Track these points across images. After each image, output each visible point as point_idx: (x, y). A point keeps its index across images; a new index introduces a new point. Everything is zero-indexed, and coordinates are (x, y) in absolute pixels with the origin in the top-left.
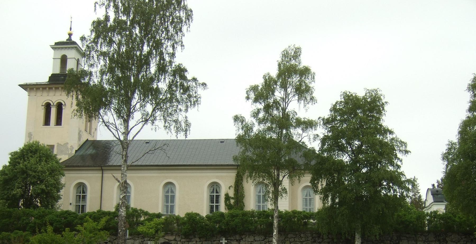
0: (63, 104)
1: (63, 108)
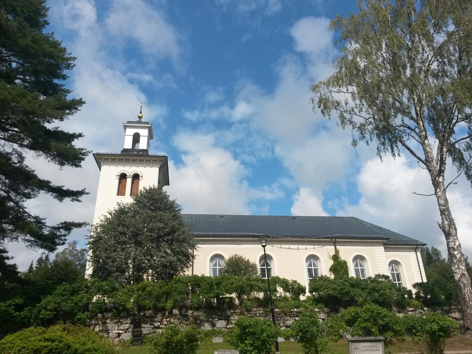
0: (141, 175)
1: (140, 179)
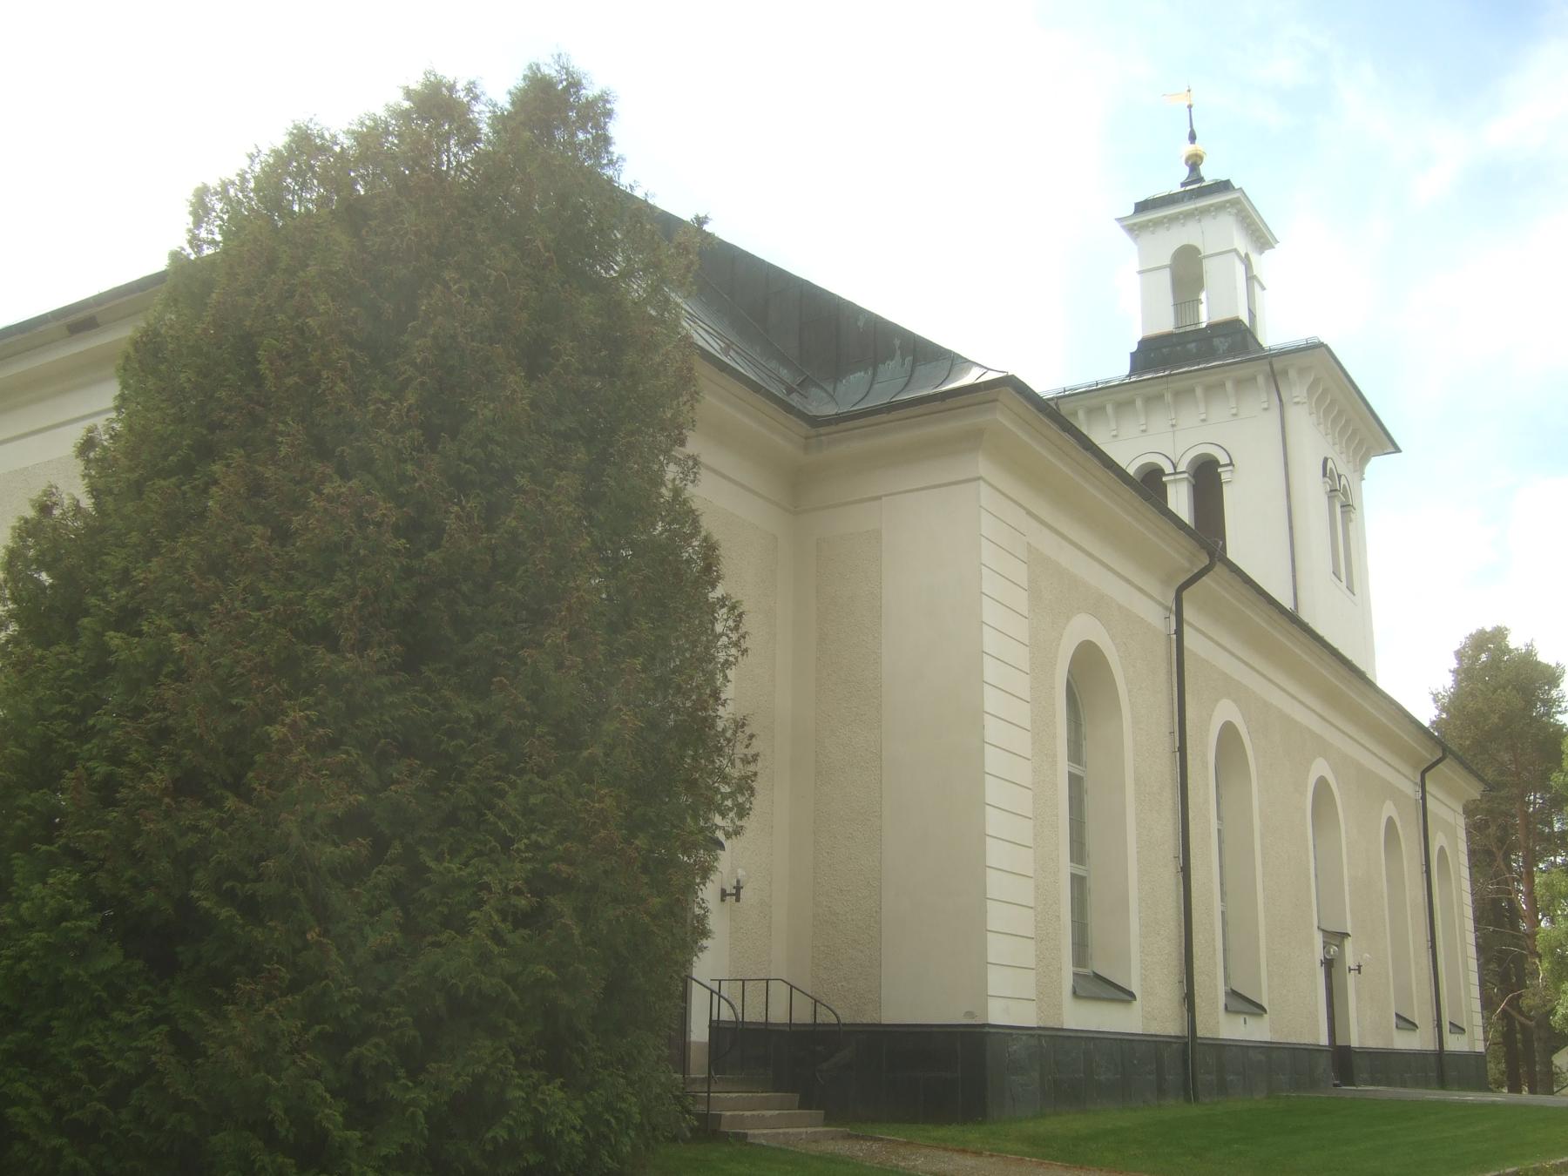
0: (1223, 459)
1: (1224, 477)
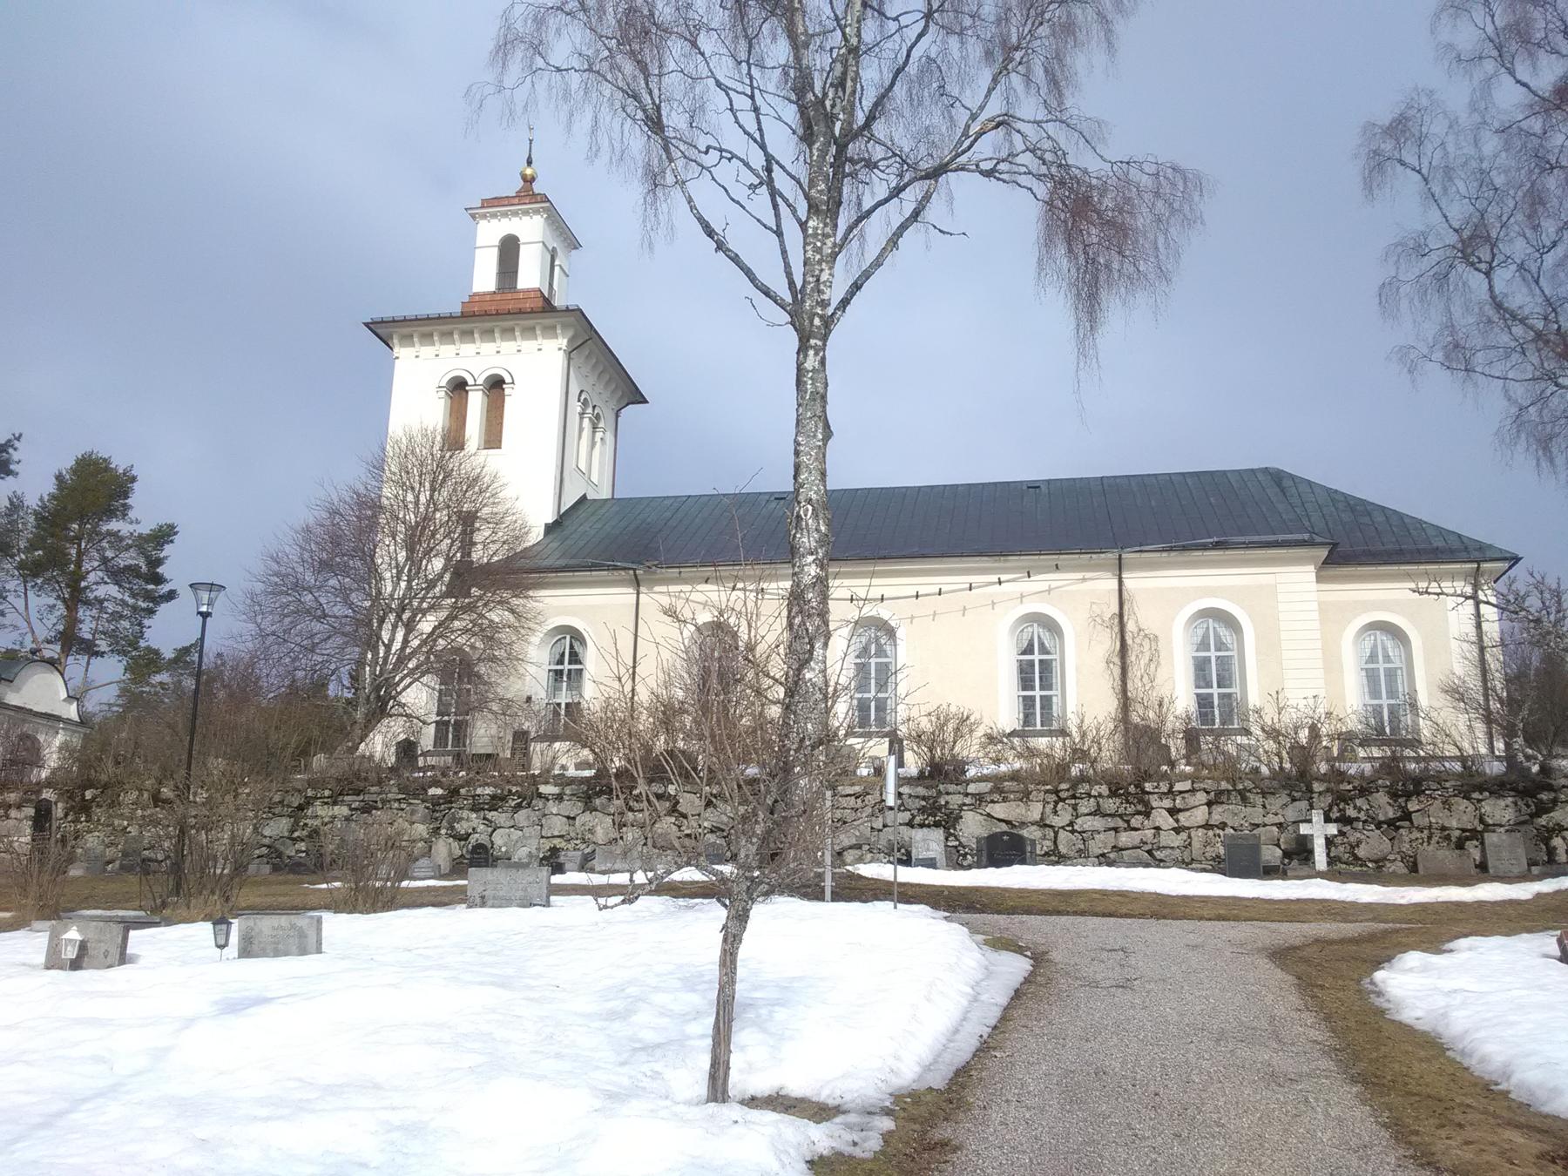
0: (508, 379)
1: (507, 392)
